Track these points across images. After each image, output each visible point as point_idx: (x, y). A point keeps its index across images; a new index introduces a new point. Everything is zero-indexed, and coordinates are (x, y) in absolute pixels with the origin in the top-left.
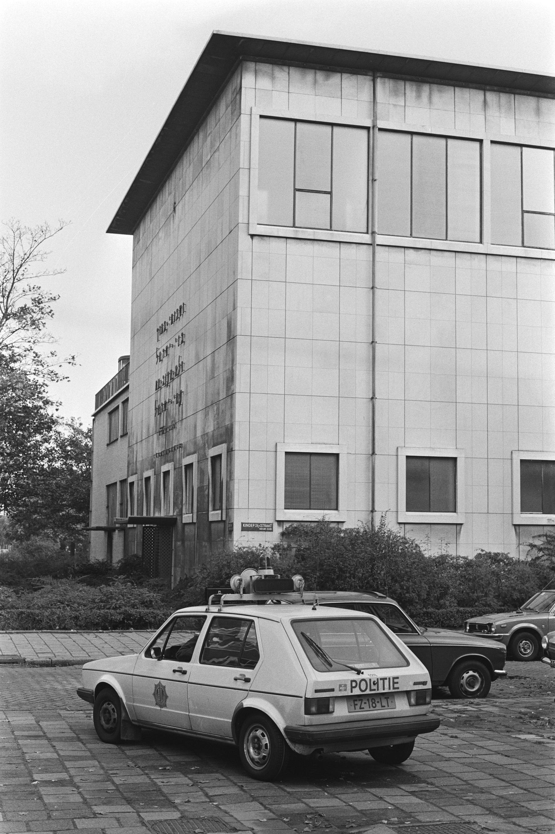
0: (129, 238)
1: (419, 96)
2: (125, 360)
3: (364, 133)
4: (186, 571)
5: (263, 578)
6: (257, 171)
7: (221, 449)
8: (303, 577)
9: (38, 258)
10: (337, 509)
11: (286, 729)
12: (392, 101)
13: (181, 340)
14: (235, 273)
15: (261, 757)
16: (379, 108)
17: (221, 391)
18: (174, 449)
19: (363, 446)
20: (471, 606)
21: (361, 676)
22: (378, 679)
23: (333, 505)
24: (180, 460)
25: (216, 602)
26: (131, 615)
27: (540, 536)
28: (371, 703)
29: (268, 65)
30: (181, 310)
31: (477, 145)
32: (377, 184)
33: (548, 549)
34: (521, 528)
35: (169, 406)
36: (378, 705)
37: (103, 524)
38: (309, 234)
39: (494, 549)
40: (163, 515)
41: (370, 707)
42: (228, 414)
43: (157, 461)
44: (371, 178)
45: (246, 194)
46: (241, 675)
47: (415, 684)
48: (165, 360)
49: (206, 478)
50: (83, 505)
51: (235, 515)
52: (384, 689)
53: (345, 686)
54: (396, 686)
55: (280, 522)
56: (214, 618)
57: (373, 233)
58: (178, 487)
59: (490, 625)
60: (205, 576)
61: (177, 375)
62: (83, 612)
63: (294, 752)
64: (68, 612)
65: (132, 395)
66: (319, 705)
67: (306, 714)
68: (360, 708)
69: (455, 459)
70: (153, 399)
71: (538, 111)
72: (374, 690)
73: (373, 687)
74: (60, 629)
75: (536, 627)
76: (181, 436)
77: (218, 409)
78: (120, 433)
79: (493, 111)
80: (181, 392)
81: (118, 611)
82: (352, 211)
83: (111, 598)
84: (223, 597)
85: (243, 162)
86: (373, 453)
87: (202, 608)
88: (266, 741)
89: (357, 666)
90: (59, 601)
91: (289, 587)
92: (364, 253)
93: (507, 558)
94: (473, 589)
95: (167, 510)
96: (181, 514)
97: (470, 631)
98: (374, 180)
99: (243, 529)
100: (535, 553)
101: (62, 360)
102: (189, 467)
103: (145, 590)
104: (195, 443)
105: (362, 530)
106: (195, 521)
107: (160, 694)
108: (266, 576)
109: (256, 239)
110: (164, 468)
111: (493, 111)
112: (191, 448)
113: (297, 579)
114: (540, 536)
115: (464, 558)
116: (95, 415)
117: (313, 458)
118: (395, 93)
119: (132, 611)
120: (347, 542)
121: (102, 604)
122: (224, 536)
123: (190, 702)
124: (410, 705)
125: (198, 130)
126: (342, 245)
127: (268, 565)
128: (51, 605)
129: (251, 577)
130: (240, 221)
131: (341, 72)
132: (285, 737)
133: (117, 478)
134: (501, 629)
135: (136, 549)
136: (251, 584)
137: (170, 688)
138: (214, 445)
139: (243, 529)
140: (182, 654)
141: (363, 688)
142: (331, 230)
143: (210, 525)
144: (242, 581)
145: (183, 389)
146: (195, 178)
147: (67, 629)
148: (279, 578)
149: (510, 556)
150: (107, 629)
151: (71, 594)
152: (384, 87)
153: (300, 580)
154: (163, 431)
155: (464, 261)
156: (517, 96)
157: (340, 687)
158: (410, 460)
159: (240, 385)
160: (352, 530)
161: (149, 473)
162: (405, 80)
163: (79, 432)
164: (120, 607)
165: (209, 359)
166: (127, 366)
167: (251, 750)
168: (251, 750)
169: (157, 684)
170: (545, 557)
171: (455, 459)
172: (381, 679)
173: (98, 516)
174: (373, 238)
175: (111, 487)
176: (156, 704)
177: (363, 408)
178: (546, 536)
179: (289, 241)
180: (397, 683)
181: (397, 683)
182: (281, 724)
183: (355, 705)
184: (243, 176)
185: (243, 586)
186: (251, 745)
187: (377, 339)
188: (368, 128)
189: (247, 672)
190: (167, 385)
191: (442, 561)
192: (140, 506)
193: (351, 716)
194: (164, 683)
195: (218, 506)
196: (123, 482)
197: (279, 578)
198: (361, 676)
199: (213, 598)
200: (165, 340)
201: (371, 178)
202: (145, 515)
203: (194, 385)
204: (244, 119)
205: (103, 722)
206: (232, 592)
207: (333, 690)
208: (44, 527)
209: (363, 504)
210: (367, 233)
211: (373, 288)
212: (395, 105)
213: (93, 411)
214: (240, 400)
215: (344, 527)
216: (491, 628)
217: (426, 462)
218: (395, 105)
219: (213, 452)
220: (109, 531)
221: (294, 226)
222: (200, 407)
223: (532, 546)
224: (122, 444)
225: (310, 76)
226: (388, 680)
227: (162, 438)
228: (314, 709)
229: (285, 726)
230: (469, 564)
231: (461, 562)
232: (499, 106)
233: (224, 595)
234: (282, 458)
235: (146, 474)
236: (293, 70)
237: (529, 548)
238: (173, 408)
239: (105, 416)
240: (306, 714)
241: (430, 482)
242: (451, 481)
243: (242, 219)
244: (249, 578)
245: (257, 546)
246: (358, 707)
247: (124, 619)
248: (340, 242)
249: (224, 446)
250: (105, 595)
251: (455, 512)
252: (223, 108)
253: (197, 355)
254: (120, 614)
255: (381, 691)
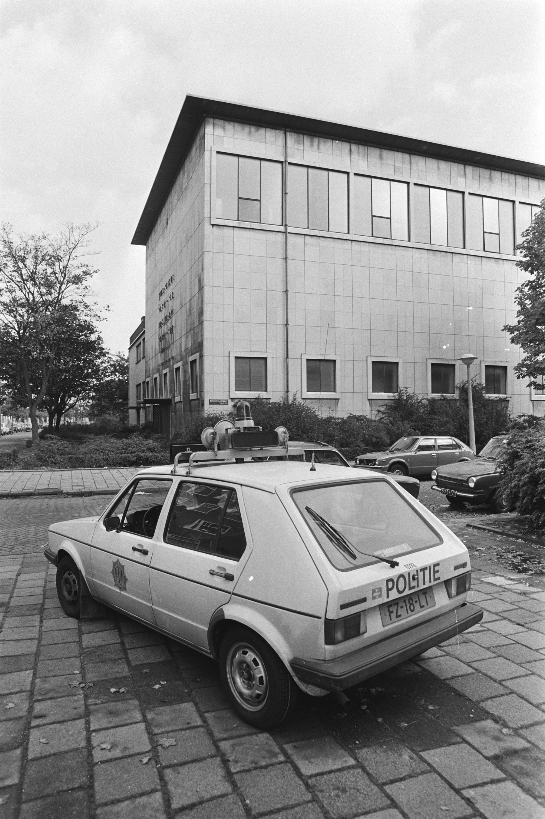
0: (143, 247)
1: (312, 144)
2: (143, 318)
3: (279, 166)
4: (177, 430)
5: (242, 431)
6: (215, 186)
7: (196, 356)
8: (287, 428)
9: (84, 244)
10: (266, 391)
11: (294, 662)
12: (296, 147)
13: (172, 297)
14: (202, 248)
15: (254, 696)
16: (289, 150)
17: (195, 321)
18: (169, 360)
19: (281, 353)
20: (347, 446)
21: (397, 571)
22: (417, 571)
23: (264, 389)
24: (173, 366)
25: (185, 459)
26: (141, 457)
27: (383, 405)
28: (408, 605)
29: (221, 121)
30: (172, 279)
31: (346, 175)
32: (288, 196)
33: (388, 413)
34: (372, 401)
35: (166, 336)
36: (417, 606)
37: (135, 405)
38: (247, 225)
39: (358, 414)
40: (164, 398)
41: (408, 613)
42: (200, 334)
43: (161, 368)
44: (284, 193)
45: (209, 199)
46: (219, 567)
47: (456, 568)
48: (163, 310)
49: (187, 375)
50: (126, 397)
51: (205, 395)
52: (424, 584)
53: (380, 589)
54: (437, 575)
55: (232, 399)
56: (181, 483)
57: (286, 225)
58: (172, 382)
59: (375, 460)
60: (188, 432)
61: (170, 317)
62: (112, 456)
63: (306, 694)
64: (102, 456)
65: (147, 336)
66: (344, 627)
67: (327, 643)
68: (398, 616)
69: (334, 361)
70: (158, 334)
71: (381, 157)
72: (414, 587)
73: (413, 583)
74: (96, 467)
75: (404, 461)
76: (174, 352)
77: (194, 332)
78: (142, 357)
79: (355, 156)
80: (172, 326)
81: (133, 455)
82: (272, 214)
83: (129, 447)
84: (192, 456)
85: (207, 181)
86: (287, 357)
87: (166, 469)
88: (260, 671)
89: (387, 553)
90: (96, 450)
91: (274, 440)
92: (280, 237)
93: (366, 418)
94: (349, 437)
95: (166, 395)
96: (174, 397)
97: (360, 464)
98: (286, 193)
99: (210, 403)
100: (382, 416)
101: (101, 308)
102: (178, 369)
103: (151, 441)
104: (181, 355)
105: (282, 403)
106: (182, 400)
107: (119, 573)
108: (245, 428)
109: (215, 227)
110: (164, 372)
111: (355, 156)
112: (178, 358)
113: (281, 430)
114: (383, 405)
115: (341, 418)
116: (129, 349)
117: (252, 360)
118: (298, 142)
119: (142, 455)
120: (274, 410)
121: (123, 451)
122: (199, 407)
123: (154, 593)
124: (450, 596)
125: (180, 171)
126: (267, 232)
127: (247, 415)
128: (91, 452)
129: (227, 430)
130: (206, 182)
131: (266, 127)
132: (292, 673)
133: (141, 381)
134: (381, 463)
135: (150, 418)
136: (227, 438)
137: (130, 569)
138: (192, 355)
139: (210, 403)
140: (142, 523)
141: (401, 588)
142: (260, 223)
143: (190, 403)
144: (216, 434)
145: (173, 325)
146: (178, 201)
147: (101, 467)
148: (261, 430)
149: (367, 417)
150: (126, 466)
151: (105, 445)
152: (291, 138)
153: (285, 433)
154: (163, 351)
155: (338, 244)
156: (369, 148)
157: (373, 593)
158: (309, 361)
159: (207, 316)
160: (276, 403)
161: (157, 375)
162: (304, 134)
163: (123, 359)
164: (135, 452)
165: (188, 305)
166: (144, 320)
167: (238, 680)
168: (238, 680)
169: (115, 561)
170: (386, 418)
171: (334, 361)
172: (421, 570)
173: (133, 402)
174: (286, 229)
175: (138, 386)
176: (116, 585)
177: (281, 330)
178: (386, 405)
179: (236, 229)
180: (438, 571)
181: (438, 571)
182: (285, 654)
183: (390, 613)
184: (207, 189)
185: (217, 441)
186: (238, 675)
187: (289, 289)
188: (281, 162)
189: (229, 564)
190: (164, 324)
191: (329, 420)
192: (152, 394)
193: (386, 631)
194: (122, 561)
195: (194, 391)
196: (144, 382)
197: (261, 430)
198: (397, 571)
199: (180, 457)
200: (164, 298)
201: (284, 193)
202: (155, 398)
203: (180, 322)
204: (207, 153)
205: (66, 593)
206: (203, 449)
207: (364, 600)
208: (108, 409)
209: (281, 388)
210: (282, 225)
211: (286, 258)
212: (298, 149)
213: (129, 346)
214: (206, 325)
215: (271, 401)
216: (375, 462)
217: (318, 363)
218: (298, 149)
219: (191, 359)
220: (138, 409)
221: (238, 220)
222: (183, 333)
223: (379, 411)
224: (143, 362)
225: (247, 129)
226: (428, 570)
227: (163, 355)
228: (339, 635)
229: (291, 657)
230: (344, 422)
231: (340, 421)
232: (359, 153)
233: (194, 453)
234: (233, 360)
235: (155, 376)
236: (236, 125)
237: (377, 412)
238: (168, 337)
239: (134, 348)
240: (327, 643)
241: (321, 373)
242: (332, 373)
243: (206, 215)
244: (224, 431)
245: (219, 413)
246: (393, 615)
247: (136, 460)
248: (266, 230)
249: (198, 354)
250: (125, 445)
251: (335, 392)
252: (194, 152)
253: (181, 303)
254: (134, 456)
255: (422, 587)
